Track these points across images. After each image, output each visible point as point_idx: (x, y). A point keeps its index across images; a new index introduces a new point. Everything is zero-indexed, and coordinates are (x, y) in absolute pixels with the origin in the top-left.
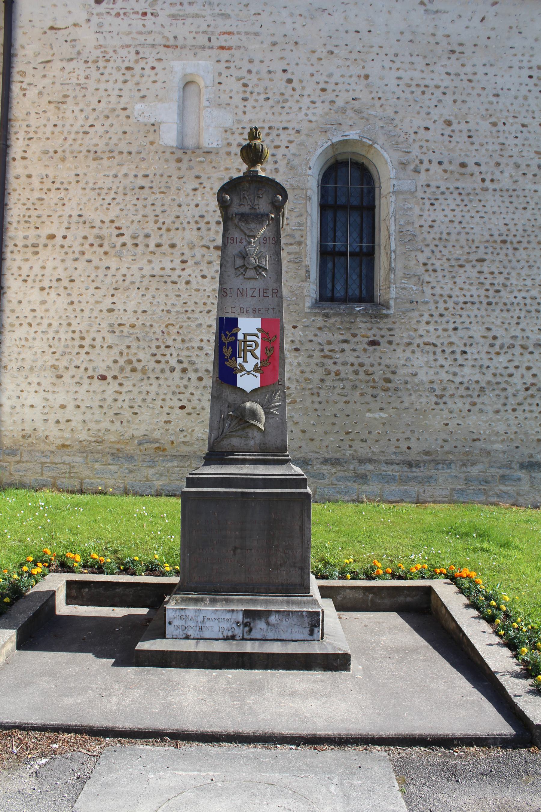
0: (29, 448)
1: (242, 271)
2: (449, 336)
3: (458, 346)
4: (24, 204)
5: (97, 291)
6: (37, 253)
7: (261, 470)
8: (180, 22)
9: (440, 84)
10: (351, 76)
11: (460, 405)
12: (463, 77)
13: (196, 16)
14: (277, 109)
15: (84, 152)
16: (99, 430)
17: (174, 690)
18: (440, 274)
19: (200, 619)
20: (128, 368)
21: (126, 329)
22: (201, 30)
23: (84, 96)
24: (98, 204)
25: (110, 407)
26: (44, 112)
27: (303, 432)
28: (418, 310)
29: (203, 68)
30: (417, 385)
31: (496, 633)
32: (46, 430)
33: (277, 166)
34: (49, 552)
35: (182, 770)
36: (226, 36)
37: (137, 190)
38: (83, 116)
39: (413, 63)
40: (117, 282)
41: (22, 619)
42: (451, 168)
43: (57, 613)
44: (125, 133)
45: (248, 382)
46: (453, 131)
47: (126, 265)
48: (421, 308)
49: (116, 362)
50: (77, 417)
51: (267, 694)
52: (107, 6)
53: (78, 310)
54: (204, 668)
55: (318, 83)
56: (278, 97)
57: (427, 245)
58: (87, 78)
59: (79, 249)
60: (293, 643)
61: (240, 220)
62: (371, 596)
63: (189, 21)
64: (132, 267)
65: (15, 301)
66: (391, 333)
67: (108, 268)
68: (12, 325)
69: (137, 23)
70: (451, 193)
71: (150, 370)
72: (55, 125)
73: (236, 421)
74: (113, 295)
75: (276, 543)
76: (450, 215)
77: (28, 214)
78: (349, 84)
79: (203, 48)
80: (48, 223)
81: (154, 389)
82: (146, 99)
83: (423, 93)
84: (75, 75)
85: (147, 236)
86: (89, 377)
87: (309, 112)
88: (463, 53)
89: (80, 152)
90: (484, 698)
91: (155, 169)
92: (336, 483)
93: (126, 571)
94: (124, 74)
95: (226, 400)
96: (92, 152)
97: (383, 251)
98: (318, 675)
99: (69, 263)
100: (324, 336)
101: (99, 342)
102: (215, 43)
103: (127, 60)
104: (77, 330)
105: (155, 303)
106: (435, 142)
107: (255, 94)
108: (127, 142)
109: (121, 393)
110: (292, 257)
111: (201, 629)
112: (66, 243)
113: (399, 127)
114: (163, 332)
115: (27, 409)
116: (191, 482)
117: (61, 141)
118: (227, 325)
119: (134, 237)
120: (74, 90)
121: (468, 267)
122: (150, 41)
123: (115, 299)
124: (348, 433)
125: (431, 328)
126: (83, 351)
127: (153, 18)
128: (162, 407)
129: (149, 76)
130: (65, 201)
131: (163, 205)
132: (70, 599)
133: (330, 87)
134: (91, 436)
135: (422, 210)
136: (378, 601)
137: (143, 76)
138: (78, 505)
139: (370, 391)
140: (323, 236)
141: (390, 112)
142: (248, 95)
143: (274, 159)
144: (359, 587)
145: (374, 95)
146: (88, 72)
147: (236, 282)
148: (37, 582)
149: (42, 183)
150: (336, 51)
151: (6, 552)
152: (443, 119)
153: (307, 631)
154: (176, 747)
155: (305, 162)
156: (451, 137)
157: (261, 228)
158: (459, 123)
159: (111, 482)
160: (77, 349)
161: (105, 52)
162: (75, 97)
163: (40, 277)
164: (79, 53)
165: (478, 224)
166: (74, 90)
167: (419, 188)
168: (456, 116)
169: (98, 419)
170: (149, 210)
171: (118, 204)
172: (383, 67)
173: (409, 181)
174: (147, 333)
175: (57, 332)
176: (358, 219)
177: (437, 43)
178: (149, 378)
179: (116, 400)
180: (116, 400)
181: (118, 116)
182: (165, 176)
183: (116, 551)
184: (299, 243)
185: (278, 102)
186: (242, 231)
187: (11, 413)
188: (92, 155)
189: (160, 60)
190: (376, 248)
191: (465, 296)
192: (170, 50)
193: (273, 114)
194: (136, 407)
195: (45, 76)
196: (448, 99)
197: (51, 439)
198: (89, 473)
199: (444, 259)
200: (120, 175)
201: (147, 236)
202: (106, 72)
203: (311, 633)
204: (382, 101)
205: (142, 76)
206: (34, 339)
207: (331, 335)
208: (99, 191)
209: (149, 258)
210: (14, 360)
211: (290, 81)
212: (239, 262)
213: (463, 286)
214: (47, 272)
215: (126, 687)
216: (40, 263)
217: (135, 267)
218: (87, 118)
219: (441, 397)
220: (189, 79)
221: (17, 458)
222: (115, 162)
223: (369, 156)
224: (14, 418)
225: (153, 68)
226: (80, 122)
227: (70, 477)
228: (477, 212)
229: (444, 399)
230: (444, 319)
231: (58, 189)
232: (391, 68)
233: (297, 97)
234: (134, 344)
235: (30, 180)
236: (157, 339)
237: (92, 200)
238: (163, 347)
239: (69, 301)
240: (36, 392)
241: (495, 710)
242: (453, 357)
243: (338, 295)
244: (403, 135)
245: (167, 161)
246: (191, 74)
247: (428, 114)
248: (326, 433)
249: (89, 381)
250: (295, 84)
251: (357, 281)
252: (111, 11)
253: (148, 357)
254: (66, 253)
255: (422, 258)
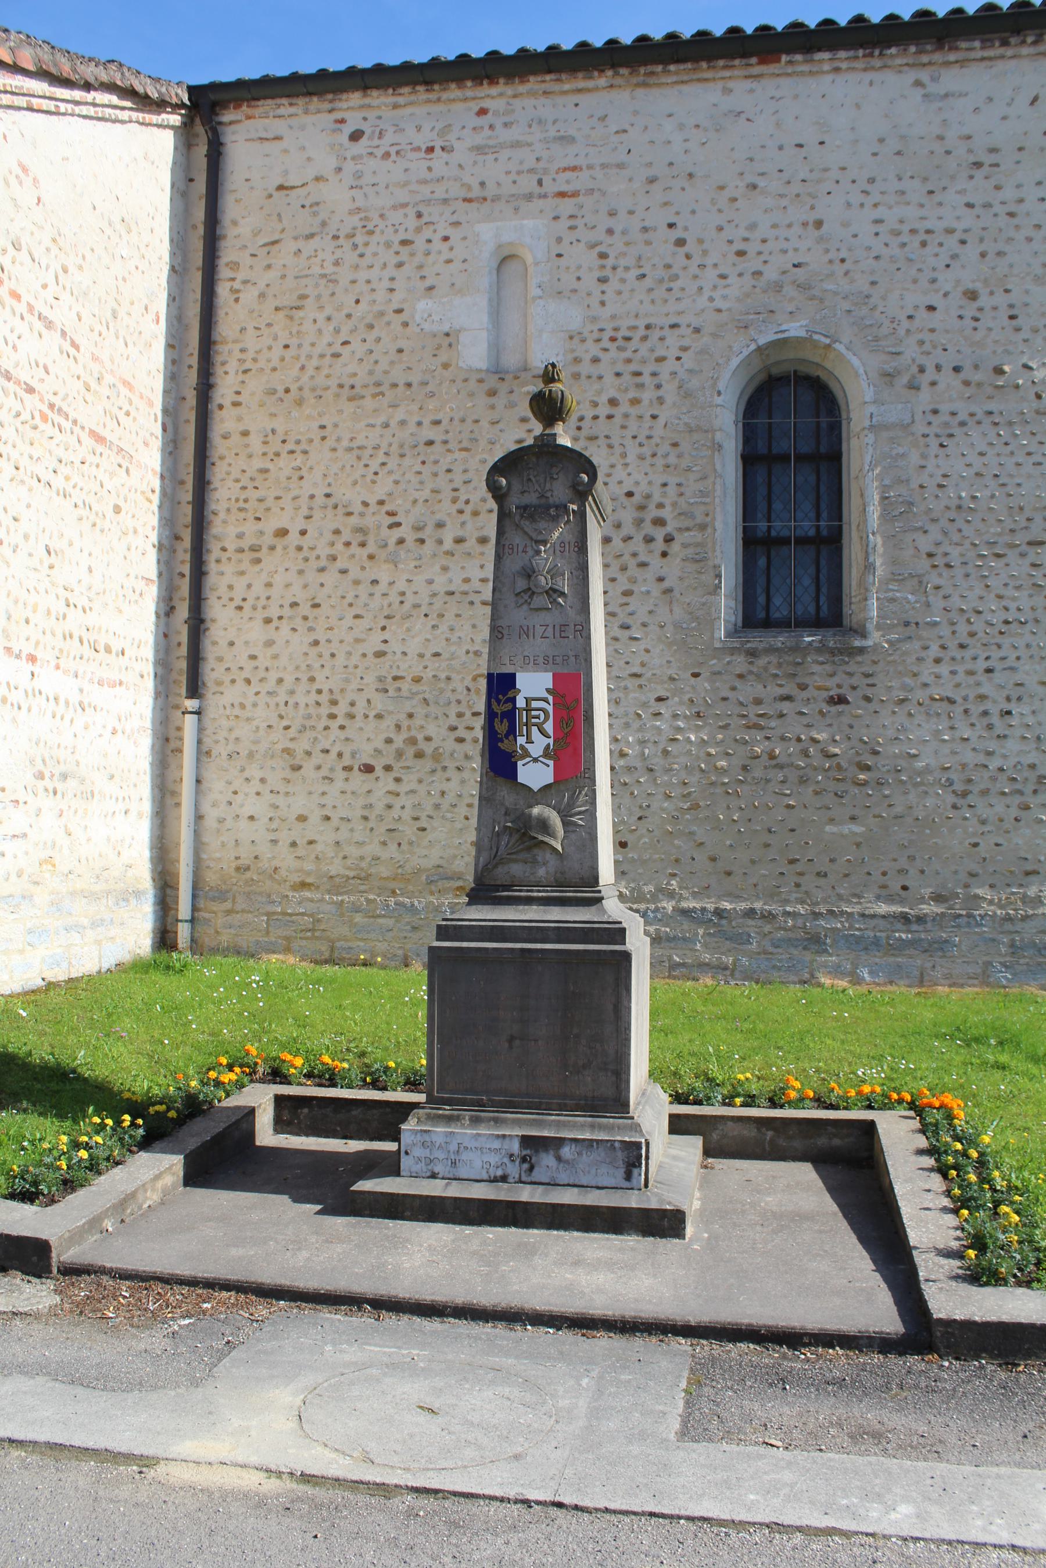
0: (247, 889)
1: (526, 597)
2: (978, 684)
3: (995, 702)
4: (237, 481)
5: (358, 621)
6: (258, 561)
7: (556, 914)
8: (491, 157)
9: (955, 224)
10: (789, 226)
11: (999, 808)
12: (998, 208)
13: (516, 145)
14: (660, 293)
15: (335, 389)
16: (362, 858)
17: (396, 1249)
18: (959, 572)
19: (453, 1147)
20: (410, 751)
21: (406, 686)
22: (526, 167)
23: (333, 294)
24: (357, 475)
25: (381, 818)
26: (269, 325)
27: (713, 859)
28: (920, 638)
29: (529, 231)
30: (919, 773)
31: (948, 1193)
32: (274, 857)
33: (660, 393)
34: (254, 1052)
35: (376, 1345)
36: (569, 174)
37: (421, 448)
38: (331, 328)
39: (903, 193)
40: (390, 605)
41: (193, 1143)
42: (977, 377)
43: (258, 1143)
44: (400, 351)
45: (535, 774)
46: (980, 309)
47: (405, 577)
48: (924, 634)
49: (389, 741)
50: (326, 837)
51: (537, 1260)
52: (369, 143)
53: (326, 655)
54: (454, 1222)
55: (730, 242)
56: (661, 273)
57: (934, 520)
58: (337, 263)
59: (328, 551)
60: (598, 1191)
61: (522, 516)
62: (770, 1134)
63: (504, 154)
64: (415, 578)
65: (223, 643)
66: (870, 681)
67: (375, 582)
68: (219, 683)
69: (418, 165)
70: (979, 423)
71: (447, 754)
72: (286, 347)
73: (516, 837)
74: (384, 628)
75: (575, 1031)
76: (977, 463)
77: (243, 497)
78: (787, 239)
79: (529, 197)
80: (275, 510)
81: (453, 787)
82: (434, 292)
83: (924, 244)
84: (318, 260)
85: (440, 525)
86: (345, 768)
87: (717, 295)
88: (997, 165)
89: (327, 388)
90: (884, 1285)
91: (452, 409)
92: (771, 949)
93: (376, 1085)
94: (397, 253)
95: (502, 804)
96: (347, 388)
97: (854, 534)
98: (631, 1241)
99: (311, 576)
100: (749, 690)
101: (360, 709)
102: (549, 187)
103: (402, 229)
104: (325, 689)
105: (454, 639)
106: (947, 331)
107: (619, 270)
108: (404, 366)
109: (398, 795)
110: (690, 552)
111: (454, 1163)
112: (306, 542)
113: (880, 309)
114: (469, 690)
115: (244, 823)
116: (443, 933)
117: (295, 372)
118: (501, 685)
119: (418, 529)
120: (317, 285)
121: (1012, 556)
122: (440, 194)
123: (386, 635)
124: (792, 862)
125: (944, 669)
126: (334, 725)
127: (445, 155)
128: (467, 818)
129: (440, 252)
130: (303, 473)
131: (465, 471)
132: (281, 1124)
133: (752, 248)
134: (349, 868)
135: (924, 456)
136: (782, 1142)
137: (428, 254)
138: (319, 982)
139: (832, 786)
140: (748, 510)
141: (862, 284)
142: (608, 272)
143: (656, 381)
144: (749, 1119)
145: (832, 255)
146: (339, 253)
147: (518, 616)
148: (228, 1095)
149: (265, 443)
150: (761, 183)
151: (188, 1050)
152: (960, 289)
153: (621, 1172)
154: (378, 1319)
155: (710, 382)
156: (977, 320)
157: (556, 527)
158: (992, 293)
159: (382, 946)
160: (325, 722)
161: (366, 218)
162: (319, 297)
163: (263, 602)
164: (324, 224)
165: (1029, 476)
166: (317, 285)
167: (918, 417)
168: (986, 282)
169: (361, 839)
170: (442, 482)
171: (390, 472)
172: (849, 205)
173: (900, 406)
174: (442, 691)
175: (292, 692)
176: (812, 478)
177: (948, 152)
178: (445, 768)
179: (389, 807)
180: (389, 807)
181: (388, 323)
182: (469, 421)
183: (363, 1054)
184: (703, 527)
185: (661, 281)
186: (526, 533)
187: (218, 831)
188: (346, 392)
189: (457, 224)
190: (845, 528)
191: (1006, 609)
192: (474, 205)
193: (653, 301)
194: (424, 818)
195: (269, 267)
196: (971, 252)
197: (283, 873)
198: (345, 930)
199: (967, 542)
200: (393, 423)
201: (440, 525)
202: (368, 251)
203: (628, 1176)
204: (847, 265)
205: (428, 254)
206: (255, 705)
207: (760, 687)
208: (359, 452)
209: (444, 562)
210: (223, 741)
211: (681, 242)
212: (521, 584)
213: (1002, 591)
214: (275, 592)
215: (327, 1241)
216: (264, 578)
217: (419, 579)
218: (337, 331)
219: (965, 794)
220: (506, 252)
221: (228, 905)
222: (385, 401)
223: (828, 365)
224: (222, 838)
225: (446, 239)
226: (327, 338)
227: (314, 938)
228: (1029, 454)
229: (971, 799)
230: (968, 654)
231: (292, 452)
232: (862, 205)
233: (694, 269)
234: (420, 711)
235: (246, 440)
236: (459, 702)
237: (348, 467)
238: (468, 714)
239: (311, 640)
240: (258, 794)
241: (892, 1300)
242: (985, 721)
243: (777, 615)
244: (887, 323)
245: (471, 395)
246: (511, 244)
247: (934, 281)
248: (753, 862)
249: (345, 774)
250: (690, 247)
251: (813, 588)
252: (375, 151)
253: (444, 732)
254: (306, 560)
255: (925, 543)
